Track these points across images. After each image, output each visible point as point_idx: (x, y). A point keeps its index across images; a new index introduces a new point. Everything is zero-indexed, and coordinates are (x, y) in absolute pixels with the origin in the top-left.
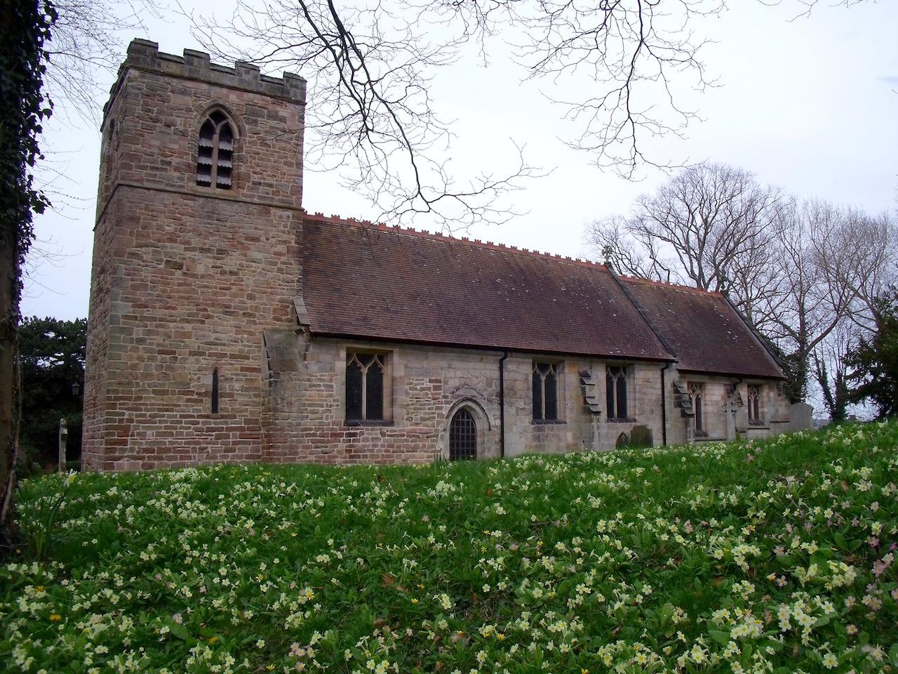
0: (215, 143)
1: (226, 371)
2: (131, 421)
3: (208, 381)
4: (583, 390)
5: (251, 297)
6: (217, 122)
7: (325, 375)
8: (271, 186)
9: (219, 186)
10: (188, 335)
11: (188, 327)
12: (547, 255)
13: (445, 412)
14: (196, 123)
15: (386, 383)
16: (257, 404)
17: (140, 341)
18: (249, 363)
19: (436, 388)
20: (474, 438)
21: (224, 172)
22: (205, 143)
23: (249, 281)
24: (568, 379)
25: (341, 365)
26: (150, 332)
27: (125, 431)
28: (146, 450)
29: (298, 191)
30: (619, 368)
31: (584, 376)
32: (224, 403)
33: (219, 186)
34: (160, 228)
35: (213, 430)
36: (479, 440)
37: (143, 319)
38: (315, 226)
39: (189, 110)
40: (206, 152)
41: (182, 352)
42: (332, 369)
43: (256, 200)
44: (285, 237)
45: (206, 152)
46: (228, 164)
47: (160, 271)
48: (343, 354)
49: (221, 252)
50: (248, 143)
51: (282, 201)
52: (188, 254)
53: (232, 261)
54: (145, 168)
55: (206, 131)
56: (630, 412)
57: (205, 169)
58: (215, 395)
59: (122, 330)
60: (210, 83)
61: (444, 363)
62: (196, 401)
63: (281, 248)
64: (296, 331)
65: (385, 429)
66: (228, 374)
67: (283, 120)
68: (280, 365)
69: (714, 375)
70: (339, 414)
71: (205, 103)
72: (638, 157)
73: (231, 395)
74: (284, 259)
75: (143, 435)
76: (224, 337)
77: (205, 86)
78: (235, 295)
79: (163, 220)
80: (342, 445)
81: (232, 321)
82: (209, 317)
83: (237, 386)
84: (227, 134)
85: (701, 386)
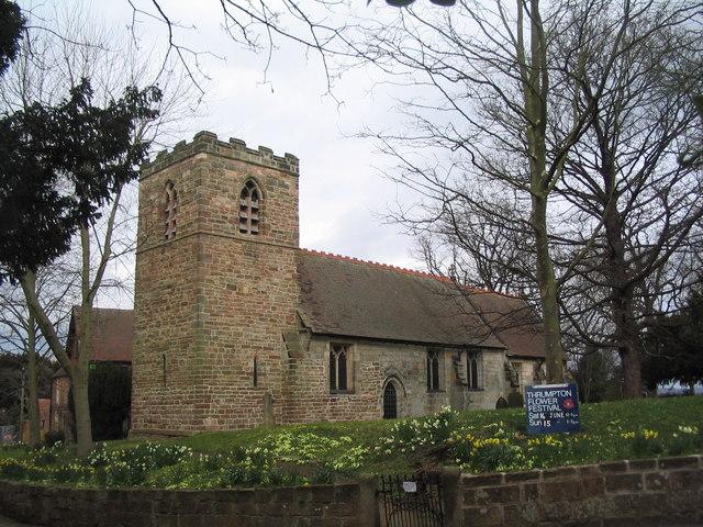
0: (249, 202)
1: (261, 359)
2: (211, 392)
3: (251, 365)
4: (456, 370)
5: (274, 309)
6: (250, 188)
7: (317, 363)
8: (282, 232)
9: (253, 233)
10: (240, 334)
11: (241, 329)
12: (385, 265)
13: (381, 385)
14: (240, 187)
15: (349, 366)
16: (278, 380)
17: (215, 338)
18: (274, 353)
19: (376, 369)
20: (395, 402)
21: (254, 222)
22: (244, 203)
23: (273, 298)
24: (446, 361)
25: (327, 354)
26: (220, 333)
27: (208, 398)
28: (220, 412)
29: (297, 236)
30: (474, 352)
31: (456, 360)
32: (261, 379)
33: (253, 233)
34: (223, 262)
35: (255, 397)
36: (398, 404)
37: (216, 324)
38: (305, 259)
39: (236, 181)
40: (243, 208)
41: (238, 347)
42: (322, 356)
43: (274, 243)
44: (291, 268)
45: (243, 208)
46: (256, 218)
47: (224, 292)
48: (328, 346)
49: (256, 278)
50: (271, 201)
51: (289, 243)
52: (239, 280)
53: (263, 285)
54: (213, 221)
55: (244, 194)
56: (479, 384)
57: (243, 220)
58: (255, 374)
59: (206, 332)
60: (248, 162)
61: (380, 352)
62: (246, 378)
63: (289, 276)
64: (301, 332)
65: (351, 396)
66: (263, 360)
67: (287, 187)
68: (294, 357)
69: (527, 358)
70: (325, 388)
71: (244, 176)
72: (450, 105)
73: (264, 374)
74: (290, 282)
75: (217, 401)
76: (260, 336)
77: (243, 165)
78: (266, 307)
79: (225, 257)
80: (329, 407)
81: (263, 325)
82: (251, 322)
83: (268, 368)
84: (255, 196)
85: (519, 365)
